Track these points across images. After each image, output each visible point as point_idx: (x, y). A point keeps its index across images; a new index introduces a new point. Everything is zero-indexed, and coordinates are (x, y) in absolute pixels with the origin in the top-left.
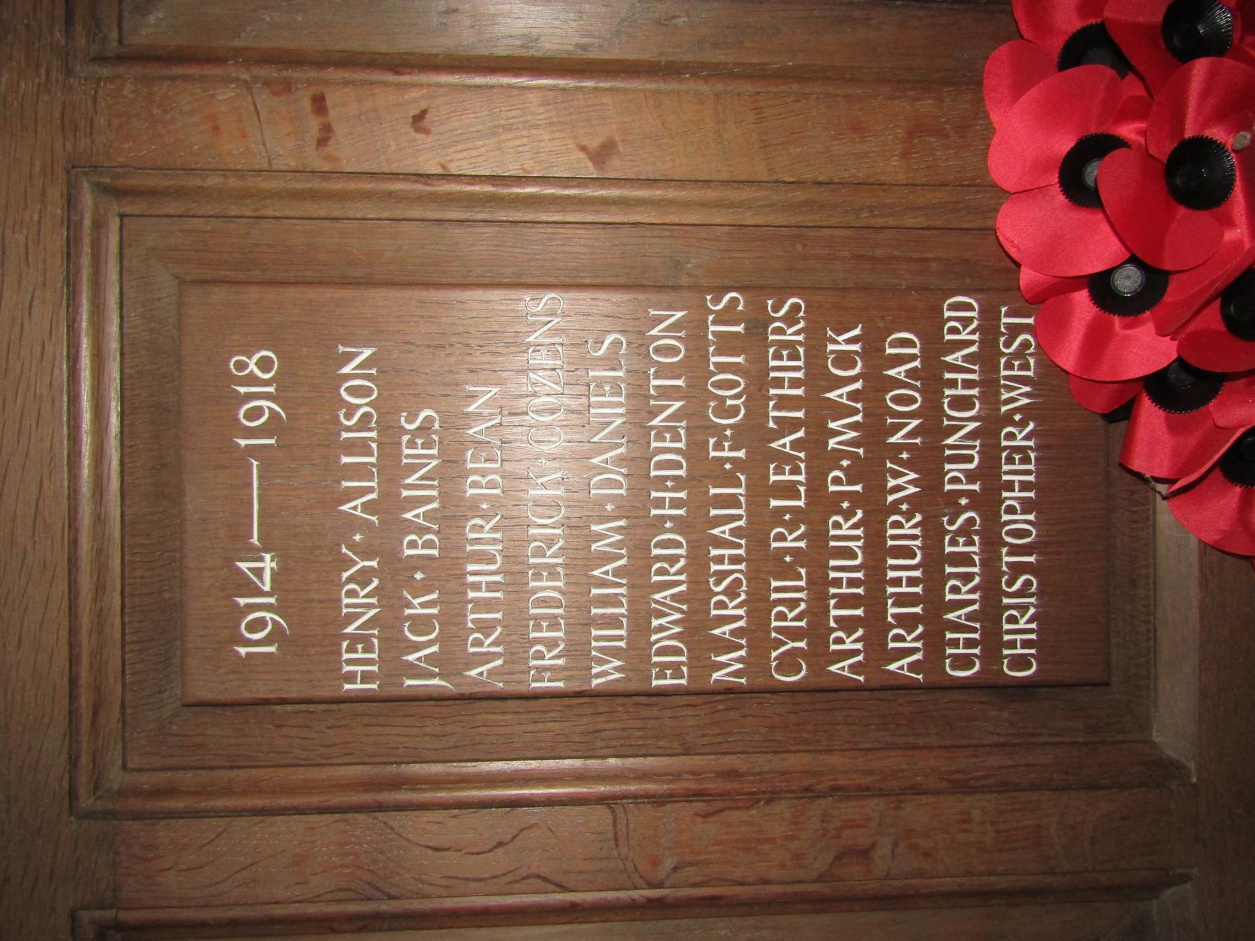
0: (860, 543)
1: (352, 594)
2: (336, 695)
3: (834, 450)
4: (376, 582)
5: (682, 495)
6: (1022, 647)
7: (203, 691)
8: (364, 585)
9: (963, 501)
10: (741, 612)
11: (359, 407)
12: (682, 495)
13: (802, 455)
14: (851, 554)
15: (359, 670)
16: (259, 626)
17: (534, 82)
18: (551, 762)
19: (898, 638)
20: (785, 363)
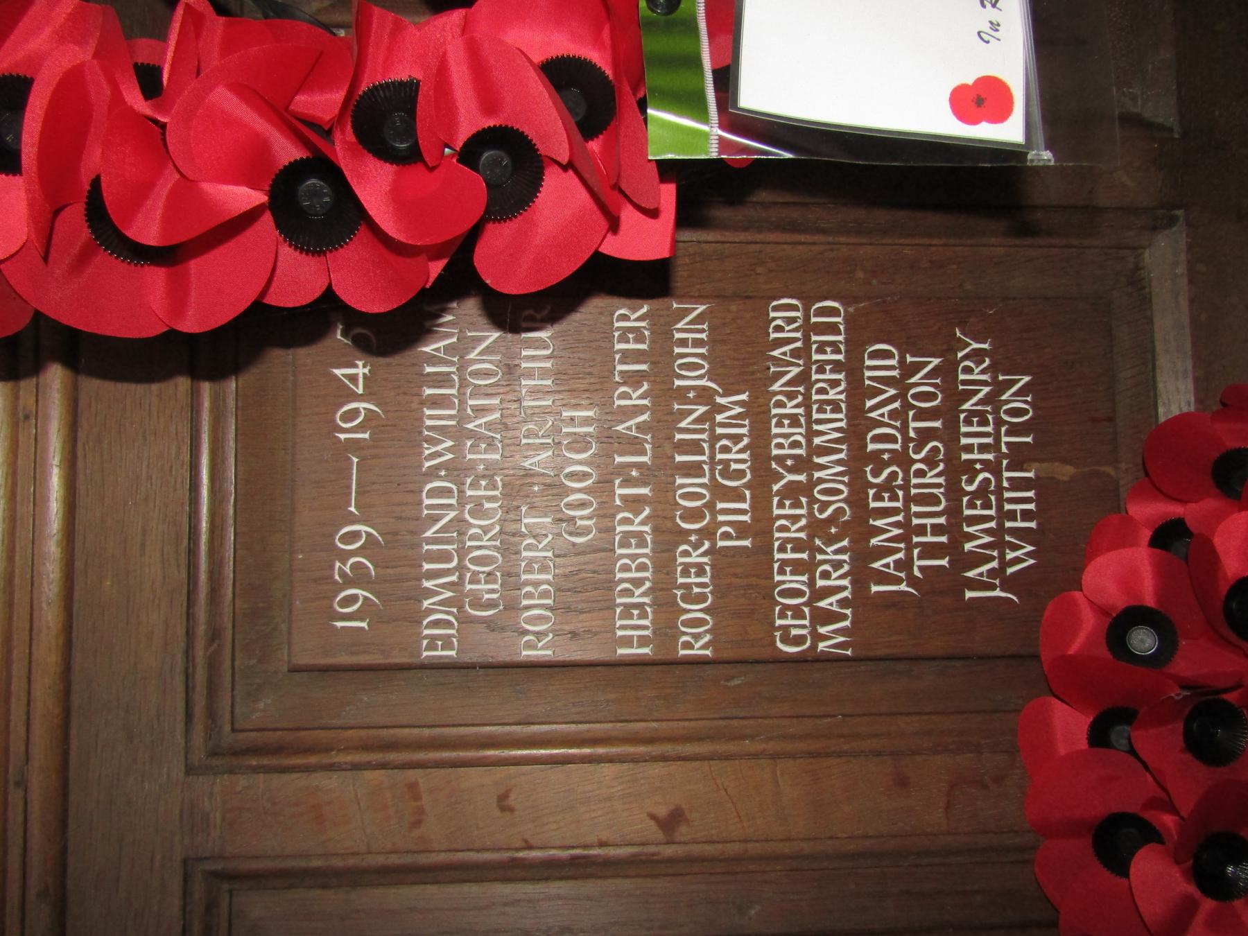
0: (942, 490)
1: (968, 370)
2: (414, 660)
3: (818, 446)
4: (987, 362)
5: (965, 456)
6: (933, 534)
7: (304, 660)
8: (978, 363)
9: (886, 456)
10: (845, 582)
11: (830, 503)
12: (965, 456)
13: (989, 408)
14: (934, 500)
15: (438, 639)
16: (351, 611)
17: (553, 852)
18: (564, 726)
19: (625, 396)
20: (828, 416)
